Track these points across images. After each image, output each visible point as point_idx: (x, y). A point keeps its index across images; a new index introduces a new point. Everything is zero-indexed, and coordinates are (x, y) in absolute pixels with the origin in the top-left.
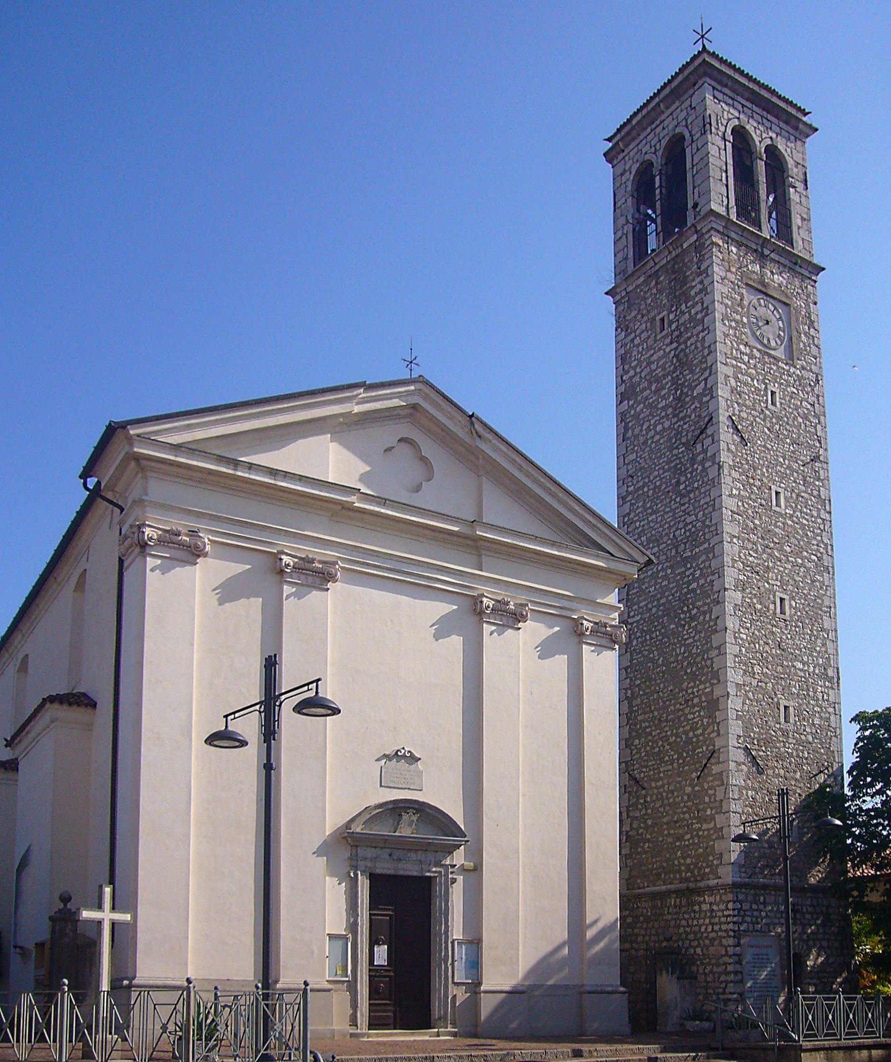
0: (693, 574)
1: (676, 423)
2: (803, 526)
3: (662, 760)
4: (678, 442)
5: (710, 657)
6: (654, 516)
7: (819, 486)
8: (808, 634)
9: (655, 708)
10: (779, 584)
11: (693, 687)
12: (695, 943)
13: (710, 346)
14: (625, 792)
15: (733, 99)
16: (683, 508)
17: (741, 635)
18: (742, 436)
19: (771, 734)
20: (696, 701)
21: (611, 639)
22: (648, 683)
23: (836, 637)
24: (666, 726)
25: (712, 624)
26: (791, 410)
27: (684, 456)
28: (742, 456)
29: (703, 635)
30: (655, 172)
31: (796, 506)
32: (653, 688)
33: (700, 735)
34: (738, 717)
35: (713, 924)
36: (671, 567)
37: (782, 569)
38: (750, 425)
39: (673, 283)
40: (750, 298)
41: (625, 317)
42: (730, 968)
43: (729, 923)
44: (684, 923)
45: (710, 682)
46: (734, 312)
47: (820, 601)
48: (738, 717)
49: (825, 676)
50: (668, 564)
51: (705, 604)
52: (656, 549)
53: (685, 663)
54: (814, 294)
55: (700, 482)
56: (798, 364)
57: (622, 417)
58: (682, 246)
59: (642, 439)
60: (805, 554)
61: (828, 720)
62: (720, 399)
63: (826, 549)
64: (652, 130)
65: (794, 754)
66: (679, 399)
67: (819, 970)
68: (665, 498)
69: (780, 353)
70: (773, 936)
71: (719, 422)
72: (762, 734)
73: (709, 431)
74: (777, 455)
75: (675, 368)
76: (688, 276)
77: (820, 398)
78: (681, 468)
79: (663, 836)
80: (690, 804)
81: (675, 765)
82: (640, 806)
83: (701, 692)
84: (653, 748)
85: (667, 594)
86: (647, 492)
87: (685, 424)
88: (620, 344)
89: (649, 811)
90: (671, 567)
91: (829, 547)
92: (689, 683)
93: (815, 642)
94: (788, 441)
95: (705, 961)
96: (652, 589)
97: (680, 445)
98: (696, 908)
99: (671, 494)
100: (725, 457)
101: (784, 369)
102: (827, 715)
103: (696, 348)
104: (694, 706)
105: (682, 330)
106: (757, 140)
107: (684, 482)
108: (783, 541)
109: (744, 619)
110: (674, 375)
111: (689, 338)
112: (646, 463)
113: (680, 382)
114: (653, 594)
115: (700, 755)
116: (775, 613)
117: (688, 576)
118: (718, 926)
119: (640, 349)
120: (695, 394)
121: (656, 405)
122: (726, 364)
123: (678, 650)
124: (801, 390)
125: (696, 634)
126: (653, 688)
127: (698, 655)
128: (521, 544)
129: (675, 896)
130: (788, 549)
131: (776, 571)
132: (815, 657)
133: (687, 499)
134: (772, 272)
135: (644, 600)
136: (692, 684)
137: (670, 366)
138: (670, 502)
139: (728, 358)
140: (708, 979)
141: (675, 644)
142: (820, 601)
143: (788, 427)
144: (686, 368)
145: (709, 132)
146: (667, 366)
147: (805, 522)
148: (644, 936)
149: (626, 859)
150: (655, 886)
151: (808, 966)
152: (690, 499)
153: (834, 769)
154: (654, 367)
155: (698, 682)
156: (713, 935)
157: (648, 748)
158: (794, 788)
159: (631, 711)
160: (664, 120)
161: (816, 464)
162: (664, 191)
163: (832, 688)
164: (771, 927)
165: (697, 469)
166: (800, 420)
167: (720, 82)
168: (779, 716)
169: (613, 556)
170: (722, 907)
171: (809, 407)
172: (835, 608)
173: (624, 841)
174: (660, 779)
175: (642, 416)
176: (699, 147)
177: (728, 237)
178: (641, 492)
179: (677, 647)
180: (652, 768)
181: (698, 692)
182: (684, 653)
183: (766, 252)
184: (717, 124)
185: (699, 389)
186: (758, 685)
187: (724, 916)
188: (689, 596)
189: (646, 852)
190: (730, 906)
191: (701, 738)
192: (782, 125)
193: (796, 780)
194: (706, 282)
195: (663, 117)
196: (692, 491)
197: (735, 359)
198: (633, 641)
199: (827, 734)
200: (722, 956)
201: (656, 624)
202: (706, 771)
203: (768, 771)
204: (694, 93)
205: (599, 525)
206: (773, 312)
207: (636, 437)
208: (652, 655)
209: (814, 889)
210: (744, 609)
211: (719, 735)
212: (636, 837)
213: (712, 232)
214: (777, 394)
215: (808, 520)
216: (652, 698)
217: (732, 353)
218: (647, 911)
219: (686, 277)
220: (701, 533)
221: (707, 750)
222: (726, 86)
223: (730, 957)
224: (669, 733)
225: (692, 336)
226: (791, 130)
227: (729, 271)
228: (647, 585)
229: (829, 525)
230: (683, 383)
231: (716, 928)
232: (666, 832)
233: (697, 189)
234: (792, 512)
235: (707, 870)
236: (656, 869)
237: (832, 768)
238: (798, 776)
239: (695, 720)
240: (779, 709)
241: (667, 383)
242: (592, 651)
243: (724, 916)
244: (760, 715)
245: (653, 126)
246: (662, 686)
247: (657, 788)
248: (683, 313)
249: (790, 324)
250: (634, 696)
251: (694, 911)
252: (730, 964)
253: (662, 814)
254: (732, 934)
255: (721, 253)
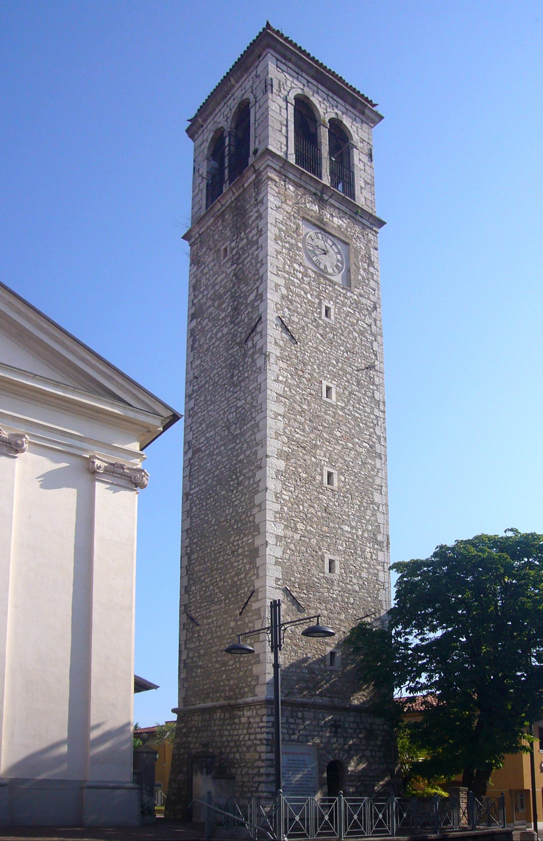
0: (241, 448)
1: (233, 328)
2: (355, 419)
3: (212, 602)
4: (234, 343)
5: (253, 513)
6: (212, 407)
7: (373, 390)
8: (357, 504)
9: (208, 560)
10: (327, 460)
11: (238, 540)
12: (235, 750)
13: (262, 260)
14: (184, 629)
15: (297, 73)
16: (235, 395)
17: (283, 496)
18: (291, 335)
19: (313, 580)
20: (240, 551)
21: (132, 481)
22: (203, 541)
23: (387, 510)
24: (216, 574)
25: (255, 486)
26: (346, 325)
27: (237, 353)
28: (291, 351)
29: (247, 497)
30: (225, 134)
31: (348, 401)
32: (207, 544)
33: (243, 579)
34: (277, 563)
35: (250, 734)
36: (225, 445)
37: (332, 449)
38: (301, 328)
39: (235, 218)
40: (306, 230)
41: (197, 254)
42: (263, 771)
43: (263, 733)
44: (226, 733)
45: (252, 534)
46: (288, 236)
47: (371, 480)
48: (277, 563)
49: (375, 541)
50: (222, 443)
51: (250, 471)
52: (213, 432)
53: (233, 521)
54: (375, 242)
55: (250, 372)
56: (356, 291)
57: (192, 334)
58: (243, 185)
59: (206, 347)
60: (357, 440)
61: (376, 575)
62: (269, 301)
63: (379, 438)
64: (225, 104)
65: (339, 599)
66: (235, 309)
67: (360, 776)
68: (222, 391)
69: (338, 278)
70: (310, 745)
71: (267, 319)
72: (304, 580)
73: (259, 329)
74: (329, 358)
75: (234, 285)
76: (248, 209)
77: (377, 322)
78: (235, 363)
79: (212, 663)
80: (234, 635)
81: (223, 605)
82: (194, 640)
83: (244, 543)
84: (205, 592)
85: (220, 467)
86: (208, 388)
87: (239, 327)
88: (193, 276)
89: (202, 643)
90: (225, 445)
91: (382, 439)
92: (235, 537)
93: (364, 512)
94: (342, 348)
95: (242, 765)
96: (208, 465)
97: (235, 345)
98: (237, 721)
99: (226, 386)
100: (271, 348)
101: (340, 291)
102: (376, 571)
103: (251, 264)
104: (239, 555)
105: (241, 253)
106: (321, 111)
107: (237, 374)
108: (333, 427)
109: (287, 483)
110: (233, 290)
111: (246, 258)
112: (208, 365)
113: (237, 295)
114: (210, 468)
115: (243, 595)
116: (321, 483)
117: (238, 450)
118: (254, 736)
119: (208, 276)
120: (248, 302)
121: (218, 317)
122: (278, 275)
123: (227, 511)
124: (358, 312)
125: (242, 497)
126: (207, 544)
127: (243, 513)
128: (15, 379)
129: (220, 711)
130: (338, 434)
131: (324, 449)
132: (364, 523)
133: (239, 388)
134: (332, 216)
135: (202, 474)
136: (238, 538)
137: (230, 285)
138: (225, 392)
139: (280, 271)
140: (244, 780)
141: (225, 506)
142: (371, 480)
143: (342, 338)
144: (242, 283)
145: (269, 91)
146: (228, 284)
147: (357, 415)
148: (195, 743)
149: (184, 682)
150: (204, 703)
151: (348, 771)
152: (241, 387)
153: (381, 615)
154: (217, 287)
155: (242, 536)
156: (249, 743)
157: (202, 593)
158: (338, 626)
159: (190, 564)
160: (234, 93)
161: (371, 372)
162: (232, 148)
163: (381, 550)
164: (309, 738)
165: (248, 361)
166: (356, 335)
167: (284, 56)
168: (323, 567)
169: (132, 406)
170: (258, 719)
171: (365, 326)
172: (386, 487)
173: (182, 667)
174: (211, 617)
175: (207, 328)
176: (261, 105)
177: (286, 176)
178: (203, 389)
179: (226, 509)
180: (204, 608)
181: (242, 543)
182: (232, 513)
183: (326, 197)
184: (280, 87)
185: (252, 297)
186: (300, 540)
187: (259, 727)
188: (237, 466)
189: (198, 676)
190: (265, 719)
191: (244, 581)
192: (348, 107)
193: (340, 620)
194: (261, 210)
195: (234, 90)
196: (243, 380)
197: (288, 273)
198: (192, 509)
199: (375, 587)
200: (256, 760)
201: (211, 492)
202: (247, 608)
203: (310, 611)
204: (258, 65)
205: (115, 377)
206: (331, 247)
207: (200, 346)
208: (207, 518)
209: (357, 709)
210: (288, 475)
211: (258, 577)
212: (192, 664)
213: (268, 169)
214: (332, 310)
215: (360, 414)
216: (206, 552)
217: (284, 268)
218: (198, 723)
219: (245, 210)
220: (249, 413)
221: (248, 591)
222: (290, 61)
223: (263, 761)
224: (218, 579)
225: (248, 256)
226: (358, 114)
227: (285, 202)
228: (205, 462)
229: (382, 421)
230: (240, 295)
231: (252, 737)
232: (214, 660)
233: (258, 138)
234: (343, 405)
235: (246, 690)
236: (206, 689)
237: (380, 614)
238: (343, 617)
239: (239, 567)
240: (323, 561)
241: (227, 298)
242: (107, 489)
243: (259, 727)
244: (302, 564)
245: (226, 100)
246: (214, 541)
247: (208, 624)
248: (242, 239)
249: (348, 260)
250: (192, 552)
251: (235, 723)
252: (262, 767)
253: (212, 645)
254: (265, 742)
255: (277, 187)
